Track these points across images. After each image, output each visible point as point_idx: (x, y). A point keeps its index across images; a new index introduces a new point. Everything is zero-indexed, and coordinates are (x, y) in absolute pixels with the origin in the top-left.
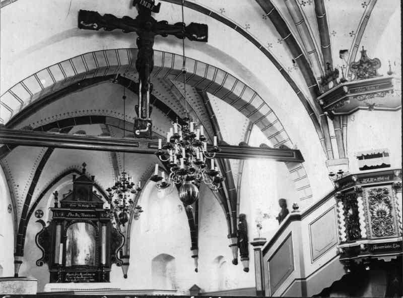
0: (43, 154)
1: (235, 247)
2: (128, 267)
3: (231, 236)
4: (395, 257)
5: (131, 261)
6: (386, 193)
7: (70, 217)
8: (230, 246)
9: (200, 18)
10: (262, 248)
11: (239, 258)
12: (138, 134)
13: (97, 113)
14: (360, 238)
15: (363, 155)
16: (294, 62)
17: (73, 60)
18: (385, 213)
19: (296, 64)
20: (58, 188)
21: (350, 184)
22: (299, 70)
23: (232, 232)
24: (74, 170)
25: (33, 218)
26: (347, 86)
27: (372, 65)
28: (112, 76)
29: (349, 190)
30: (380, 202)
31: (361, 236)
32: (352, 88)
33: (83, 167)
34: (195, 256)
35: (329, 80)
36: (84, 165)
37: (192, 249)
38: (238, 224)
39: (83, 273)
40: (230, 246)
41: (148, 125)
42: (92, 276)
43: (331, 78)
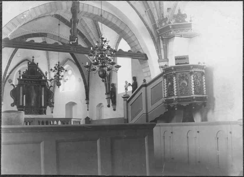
0: (12, 52)
1: (109, 99)
2: (53, 108)
3: (107, 93)
4: (188, 104)
5: (55, 105)
6: (186, 75)
7: (27, 83)
8: (106, 98)
10: (128, 99)
11: (111, 104)
12: (71, 43)
13: (43, 32)
14: (174, 95)
15: (177, 58)
16: (146, 12)
17: (95, 8)
18: (185, 84)
19: (147, 13)
20: (19, 68)
21: (171, 71)
22: (148, 15)
23: (108, 92)
24: (27, 60)
26: (171, 25)
27: (183, 17)
29: (170, 74)
30: (183, 80)
31: (174, 95)
32: (174, 27)
33: (32, 59)
34: (88, 103)
35: (163, 22)
36: (33, 57)
37: (86, 100)
38: (110, 88)
39: (33, 110)
40: (106, 98)
43: (164, 21)
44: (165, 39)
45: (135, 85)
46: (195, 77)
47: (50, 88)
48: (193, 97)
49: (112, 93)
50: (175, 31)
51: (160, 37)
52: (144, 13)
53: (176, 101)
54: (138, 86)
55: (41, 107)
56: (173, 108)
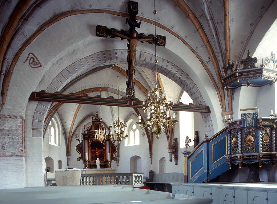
1: (170, 153)
3: (169, 148)
5: (120, 158)
8: (168, 153)
9: (160, 32)
10: (188, 156)
11: (173, 159)
16: (209, 58)
20: (85, 123)
25: (74, 139)
28: (111, 65)
34: (151, 157)
37: (150, 154)
41: (132, 92)
42: (103, 165)
44: (230, 89)
45: (197, 140)
46: (264, 132)
47: (114, 142)
48: (259, 155)
49: (174, 148)
50: (242, 79)
51: (225, 87)
52: (207, 60)
53: (241, 159)
54: (200, 141)
55: (107, 161)
56: (238, 166)
